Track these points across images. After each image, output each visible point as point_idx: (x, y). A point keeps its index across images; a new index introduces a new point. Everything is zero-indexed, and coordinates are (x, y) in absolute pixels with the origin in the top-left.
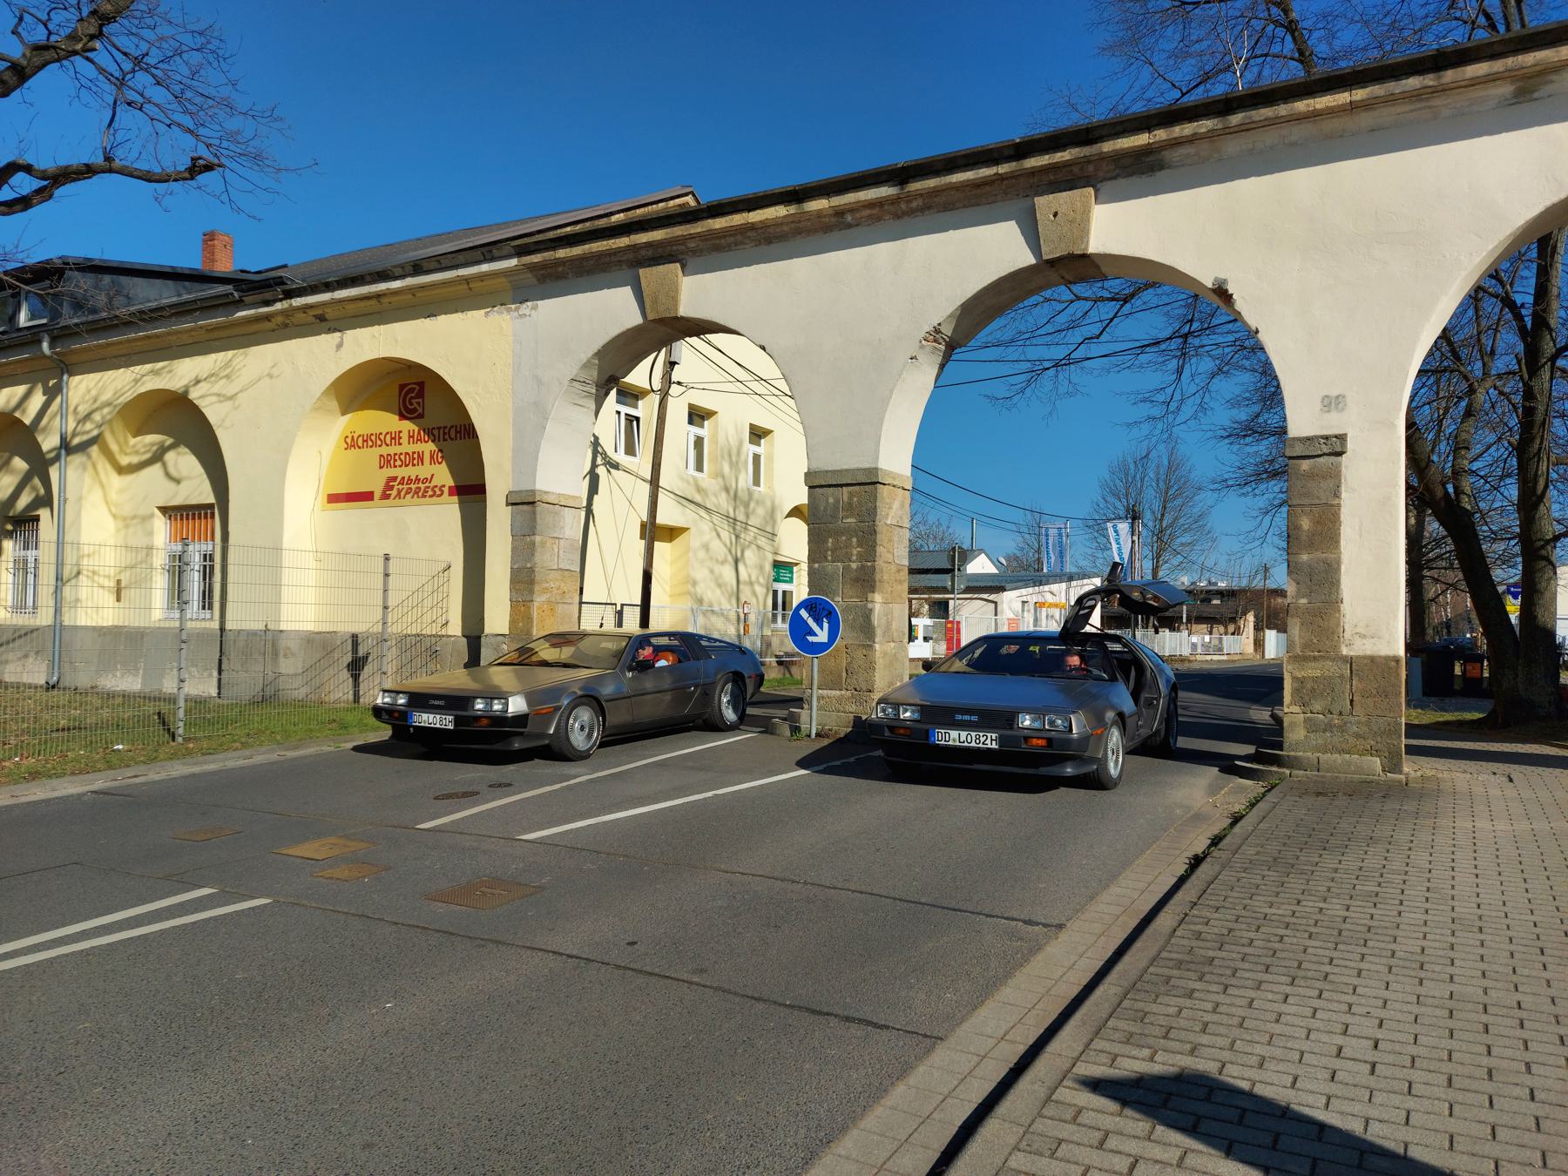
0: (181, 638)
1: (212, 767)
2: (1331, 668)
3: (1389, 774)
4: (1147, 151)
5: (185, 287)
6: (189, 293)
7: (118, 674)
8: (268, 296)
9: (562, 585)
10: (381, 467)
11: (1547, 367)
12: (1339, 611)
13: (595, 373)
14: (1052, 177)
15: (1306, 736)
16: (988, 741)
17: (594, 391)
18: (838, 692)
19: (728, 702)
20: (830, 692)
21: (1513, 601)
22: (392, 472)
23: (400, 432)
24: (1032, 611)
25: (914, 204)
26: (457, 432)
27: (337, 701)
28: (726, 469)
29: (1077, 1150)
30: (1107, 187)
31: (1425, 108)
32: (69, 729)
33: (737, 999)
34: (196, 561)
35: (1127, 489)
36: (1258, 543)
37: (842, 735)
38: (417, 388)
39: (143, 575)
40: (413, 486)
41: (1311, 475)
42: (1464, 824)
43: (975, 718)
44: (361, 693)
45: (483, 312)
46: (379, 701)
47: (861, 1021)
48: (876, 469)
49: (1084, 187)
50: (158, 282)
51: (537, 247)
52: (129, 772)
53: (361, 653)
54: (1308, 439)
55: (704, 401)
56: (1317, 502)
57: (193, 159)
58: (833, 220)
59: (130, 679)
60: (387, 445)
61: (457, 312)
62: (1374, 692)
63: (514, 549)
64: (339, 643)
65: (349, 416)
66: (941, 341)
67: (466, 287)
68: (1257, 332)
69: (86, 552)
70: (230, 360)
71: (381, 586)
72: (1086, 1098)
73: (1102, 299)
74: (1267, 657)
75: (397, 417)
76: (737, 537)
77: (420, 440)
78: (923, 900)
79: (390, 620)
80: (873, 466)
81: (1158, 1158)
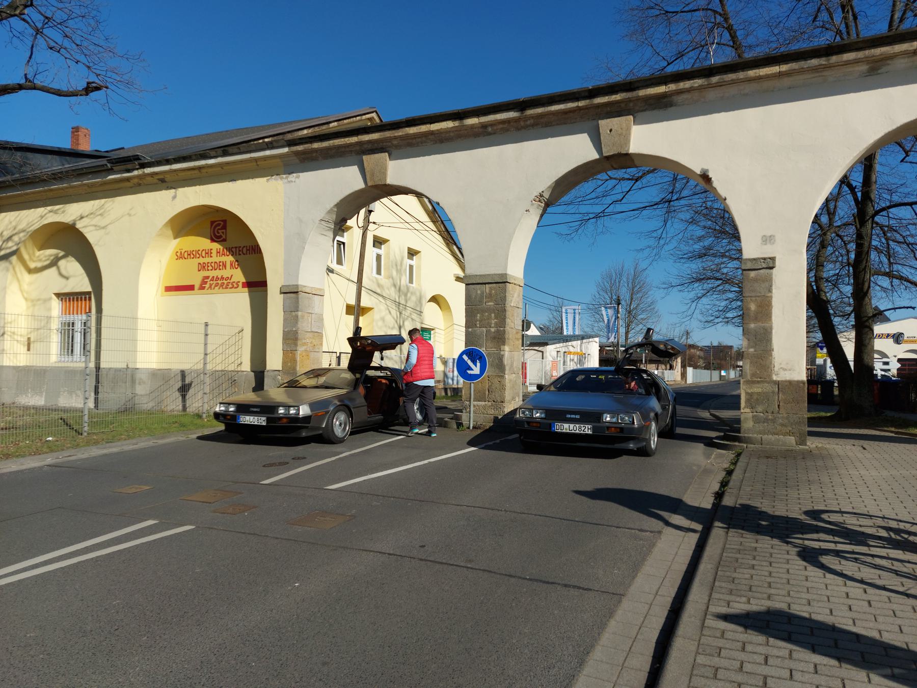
0: (70, 373)
1: (115, 450)
2: (767, 388)
3: (800, 446)
4: (664, 96)
5: (67, 161)
6: (69, 164)
7: (29, 395)
8: (129, 166)
9: (314, 341)
10: (199, 271)
11: (870, 221)
12: (771, 356)
13: (334, 216)
14: (609, 109)
15: (753, 425)
16: (586, 430)
17: (333, 227)
18: (483, 403)
19: (417, 409)
20: (478, 402)
21: (820, 351)
22: (206, 273)
23: (211, 249)
24: (562, 357)
25: (528, 122)
26: (247, 250)
27: (172, 411)
28: (394, 273)
29: (732, 653)
30: (640, 115)
31: (820, 76)
32: (9, 428)
33: (499, 576)
34: (78, 327)
35: (611, 287)
36: (689, 318)
37: (488, 428)
38: (222, 223)
39: (45, 334)
40: (220, 282)
41: (755, 280)
42: (853, 472)
43: (578, 417)
44: (187, 405)
45: (265, 179)
46: (217, 409)
47: (574, 587)
48: (506, 274)
49: (627, 115)
50: (50, 157)
51: (301, 141)
52: (66, 453)
53: (187, 381)
54: (754, 259)
55: (382, 233)
56: (759, 295)
57: (88, 83)
58: (480, 130)
59: (37, 398)
60: (203, 257)
61: (249, 178)
62: (791, 400)
63: (285, 320)
64: (173, 375)
65: (178, 240)
66: (543, 201)
67: (255, 164)
68: (725, 199)
69: (9, 320)
70: (103, 205)
71: (203, 341)
72: (723, 625)
73: (623, 179)
74: (688, 382)
75: (209, 241)
76: (401, 313)
77: (224, 254)
78: (577, 519)
79: (208, 362)
80: (504, 272)
81: (777, 655)
